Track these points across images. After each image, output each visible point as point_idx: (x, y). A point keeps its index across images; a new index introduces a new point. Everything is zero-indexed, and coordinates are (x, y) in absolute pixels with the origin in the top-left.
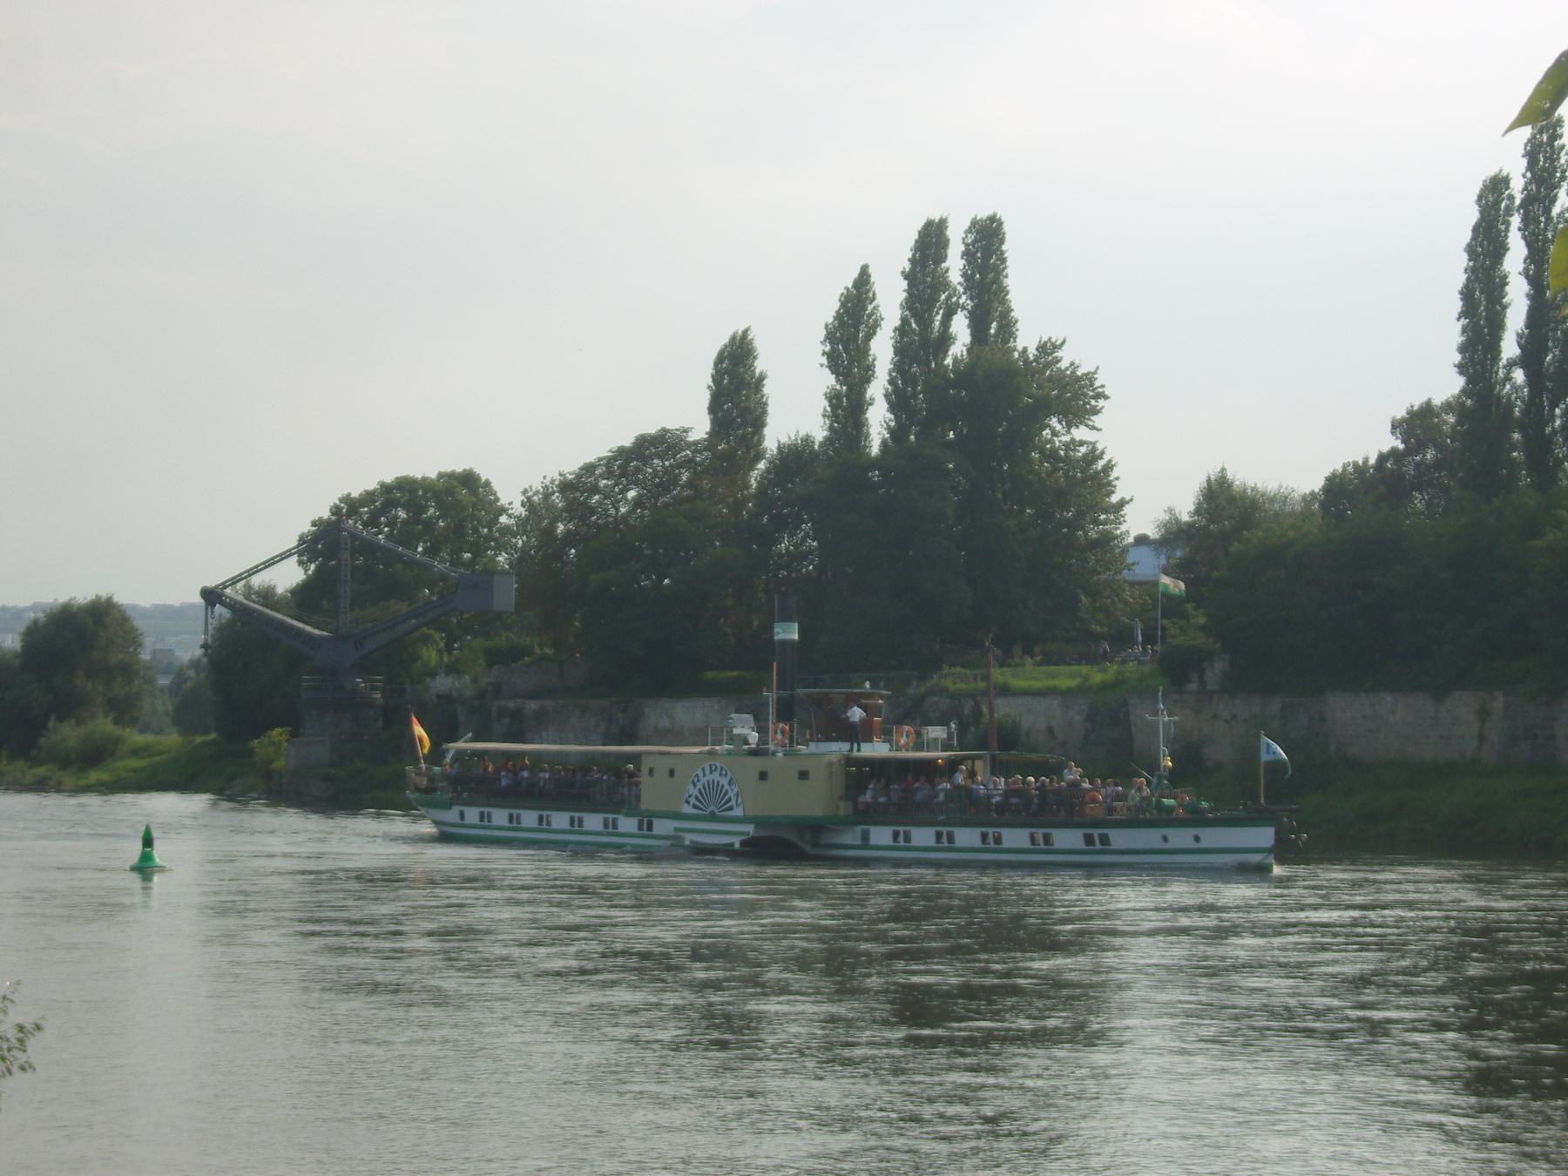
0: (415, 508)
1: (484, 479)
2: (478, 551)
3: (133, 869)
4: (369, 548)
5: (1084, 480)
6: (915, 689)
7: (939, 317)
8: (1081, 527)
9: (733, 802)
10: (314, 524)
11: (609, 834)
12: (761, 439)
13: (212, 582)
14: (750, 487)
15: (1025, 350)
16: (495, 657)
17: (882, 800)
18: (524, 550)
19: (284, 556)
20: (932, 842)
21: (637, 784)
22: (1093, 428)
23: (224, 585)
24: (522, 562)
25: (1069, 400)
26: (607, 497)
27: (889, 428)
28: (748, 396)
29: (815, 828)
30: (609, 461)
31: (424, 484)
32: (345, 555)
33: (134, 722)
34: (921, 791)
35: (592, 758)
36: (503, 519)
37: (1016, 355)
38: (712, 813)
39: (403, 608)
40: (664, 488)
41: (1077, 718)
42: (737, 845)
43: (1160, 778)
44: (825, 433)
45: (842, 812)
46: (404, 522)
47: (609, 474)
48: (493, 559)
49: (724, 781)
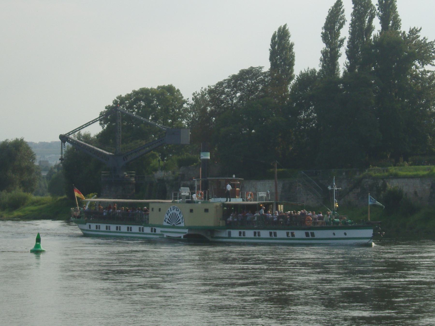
0: (148, 101)
1: (176, 89)
2: (174, 119)
3: (32, 251)
4: (129, 118)
5: (429, 87)
6: (358, 176)
7: (367, 19)
8: (429, 107)
9: (181, 221)
10: (106, 108)
11: (154, 234)
12: (292, 71)
13: (64, 133)
14: (288, 91)
15: (404, 32)
16: (182, 163)
17: (235, 220)
18: (193, 119)
19: (94, 122)
20: (268, 236)
21: (148, 214)
22: (433, 65)
23: (69, 134)
24: (192, 123)
25: (423, 53)
26: (228, 96)
27: (347, 66)
28: (286, 53)
29: (212, 231)
30: (229, 81)
31: (152, 91)
32: (119, 121)
33: (32, 191)
34: (249, 216)
35: (114, 203)
36: (185, 105)
37: (400, 35)
38: (174, 225)
39: (144, 142)
40: (251, 92)
41: (427, 188)
42: (182, 237)
43: (333, 211)
44: (320, 68)
45: (221, 225)
46: (144, 107)
47: (229, 86)
48: (180, 122)
49: (178, 213)
